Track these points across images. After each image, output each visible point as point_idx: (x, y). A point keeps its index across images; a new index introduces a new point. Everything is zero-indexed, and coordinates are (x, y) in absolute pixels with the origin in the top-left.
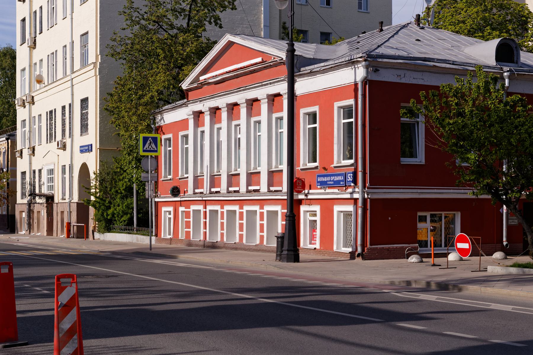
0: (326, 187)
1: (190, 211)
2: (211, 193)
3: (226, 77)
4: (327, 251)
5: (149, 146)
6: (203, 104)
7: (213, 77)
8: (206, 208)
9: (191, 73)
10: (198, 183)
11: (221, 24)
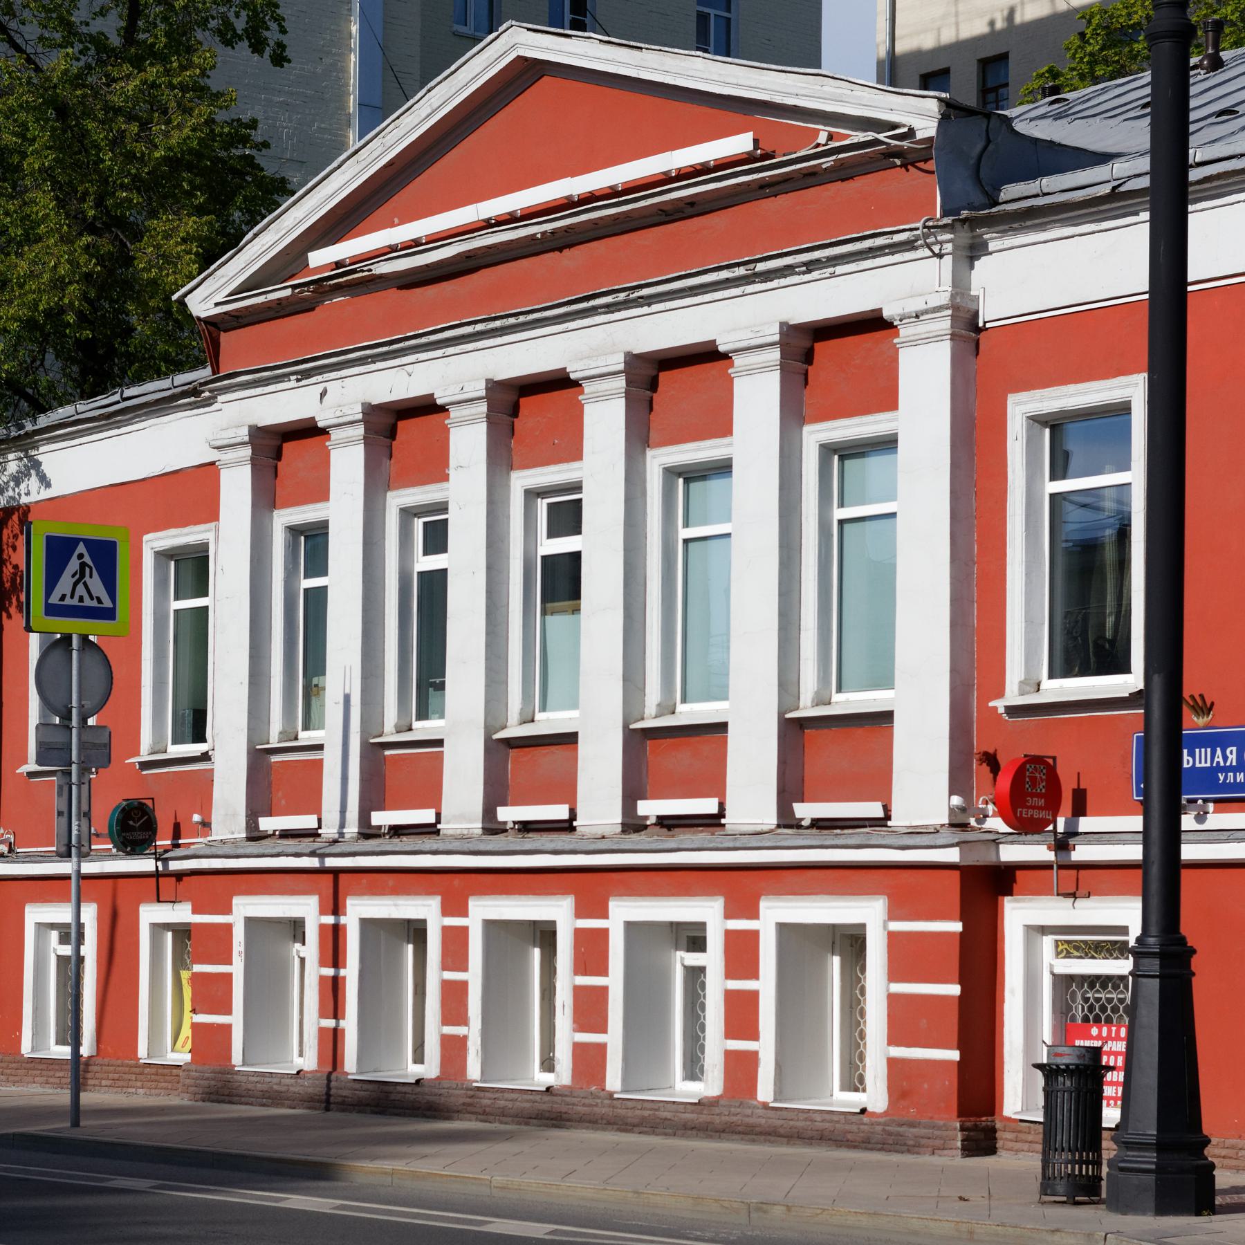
0: (1205, 801)
1: (228, 928)
2: (368, 832)
3: (489, 247)
4: (119, 1062)
5: (75, 584)
6: (320, 388)
7: (391, 250)
8: (336, 908)
9: (256, 235)
10: (270, 785)
11: (281, 46)
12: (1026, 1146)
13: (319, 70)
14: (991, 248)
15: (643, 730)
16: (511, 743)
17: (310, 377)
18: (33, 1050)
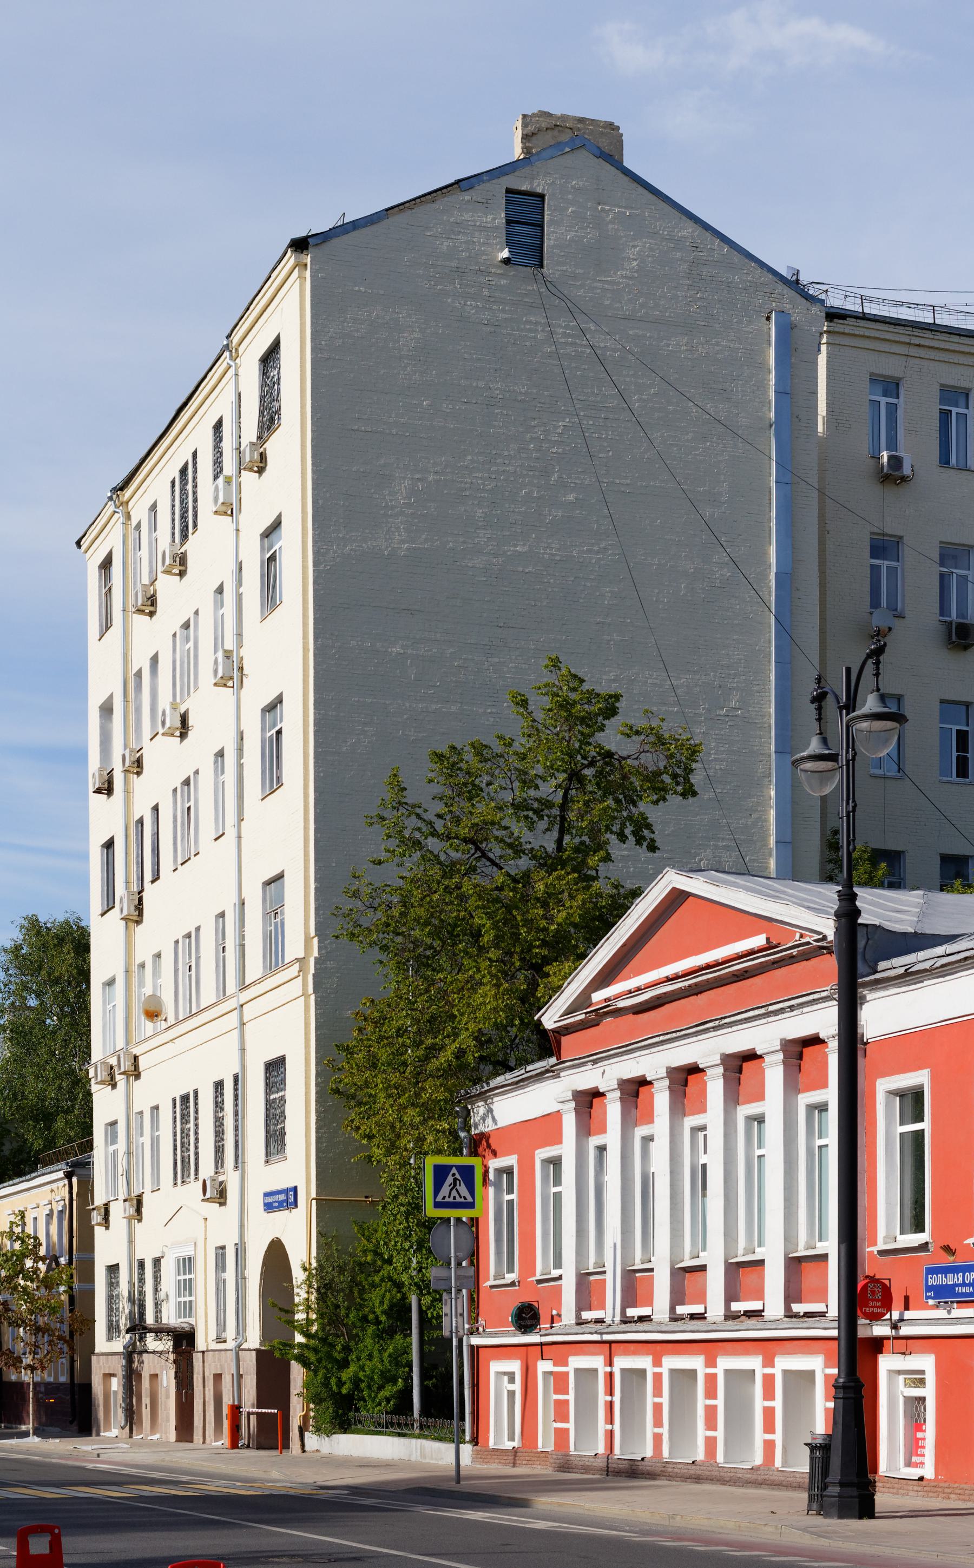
0: (952, 1302)
1: (567, 1374)
2: (626, 1321)
5: (451, 1190)
6: (601, 1070)
9: (569, 984)
10: (590, 1293)
11: (653, 840)
12: (887, 1490)
13: (749, 823)
14: (868, 999)
15: (737, 1263)
16: (799, 1260)
17: (597, 1063)
18: (495, 1444)
